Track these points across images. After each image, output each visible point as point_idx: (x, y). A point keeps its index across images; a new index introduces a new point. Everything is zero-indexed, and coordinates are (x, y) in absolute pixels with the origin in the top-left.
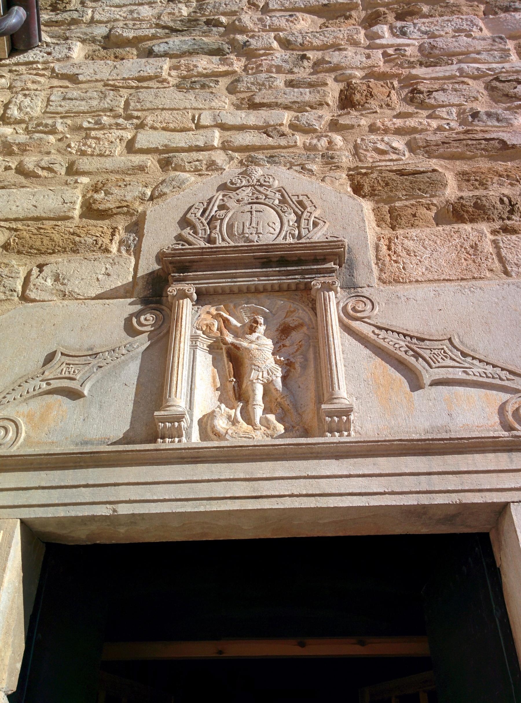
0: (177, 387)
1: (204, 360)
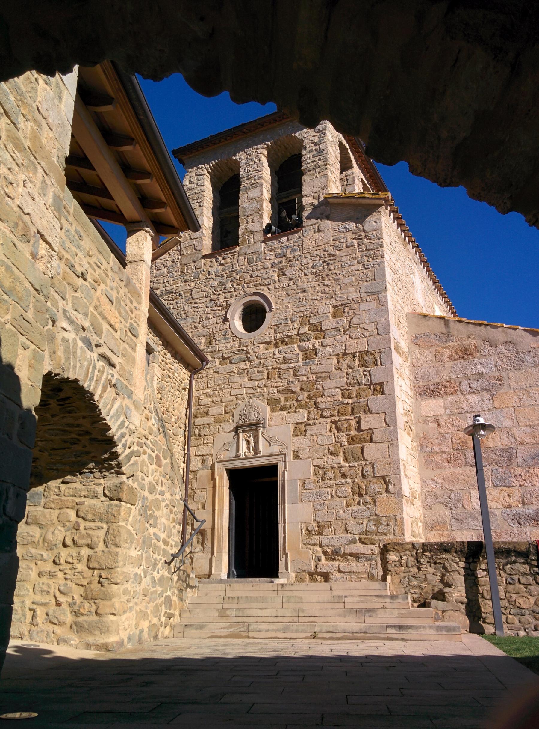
0: (183, 214)
1: (244, 442)
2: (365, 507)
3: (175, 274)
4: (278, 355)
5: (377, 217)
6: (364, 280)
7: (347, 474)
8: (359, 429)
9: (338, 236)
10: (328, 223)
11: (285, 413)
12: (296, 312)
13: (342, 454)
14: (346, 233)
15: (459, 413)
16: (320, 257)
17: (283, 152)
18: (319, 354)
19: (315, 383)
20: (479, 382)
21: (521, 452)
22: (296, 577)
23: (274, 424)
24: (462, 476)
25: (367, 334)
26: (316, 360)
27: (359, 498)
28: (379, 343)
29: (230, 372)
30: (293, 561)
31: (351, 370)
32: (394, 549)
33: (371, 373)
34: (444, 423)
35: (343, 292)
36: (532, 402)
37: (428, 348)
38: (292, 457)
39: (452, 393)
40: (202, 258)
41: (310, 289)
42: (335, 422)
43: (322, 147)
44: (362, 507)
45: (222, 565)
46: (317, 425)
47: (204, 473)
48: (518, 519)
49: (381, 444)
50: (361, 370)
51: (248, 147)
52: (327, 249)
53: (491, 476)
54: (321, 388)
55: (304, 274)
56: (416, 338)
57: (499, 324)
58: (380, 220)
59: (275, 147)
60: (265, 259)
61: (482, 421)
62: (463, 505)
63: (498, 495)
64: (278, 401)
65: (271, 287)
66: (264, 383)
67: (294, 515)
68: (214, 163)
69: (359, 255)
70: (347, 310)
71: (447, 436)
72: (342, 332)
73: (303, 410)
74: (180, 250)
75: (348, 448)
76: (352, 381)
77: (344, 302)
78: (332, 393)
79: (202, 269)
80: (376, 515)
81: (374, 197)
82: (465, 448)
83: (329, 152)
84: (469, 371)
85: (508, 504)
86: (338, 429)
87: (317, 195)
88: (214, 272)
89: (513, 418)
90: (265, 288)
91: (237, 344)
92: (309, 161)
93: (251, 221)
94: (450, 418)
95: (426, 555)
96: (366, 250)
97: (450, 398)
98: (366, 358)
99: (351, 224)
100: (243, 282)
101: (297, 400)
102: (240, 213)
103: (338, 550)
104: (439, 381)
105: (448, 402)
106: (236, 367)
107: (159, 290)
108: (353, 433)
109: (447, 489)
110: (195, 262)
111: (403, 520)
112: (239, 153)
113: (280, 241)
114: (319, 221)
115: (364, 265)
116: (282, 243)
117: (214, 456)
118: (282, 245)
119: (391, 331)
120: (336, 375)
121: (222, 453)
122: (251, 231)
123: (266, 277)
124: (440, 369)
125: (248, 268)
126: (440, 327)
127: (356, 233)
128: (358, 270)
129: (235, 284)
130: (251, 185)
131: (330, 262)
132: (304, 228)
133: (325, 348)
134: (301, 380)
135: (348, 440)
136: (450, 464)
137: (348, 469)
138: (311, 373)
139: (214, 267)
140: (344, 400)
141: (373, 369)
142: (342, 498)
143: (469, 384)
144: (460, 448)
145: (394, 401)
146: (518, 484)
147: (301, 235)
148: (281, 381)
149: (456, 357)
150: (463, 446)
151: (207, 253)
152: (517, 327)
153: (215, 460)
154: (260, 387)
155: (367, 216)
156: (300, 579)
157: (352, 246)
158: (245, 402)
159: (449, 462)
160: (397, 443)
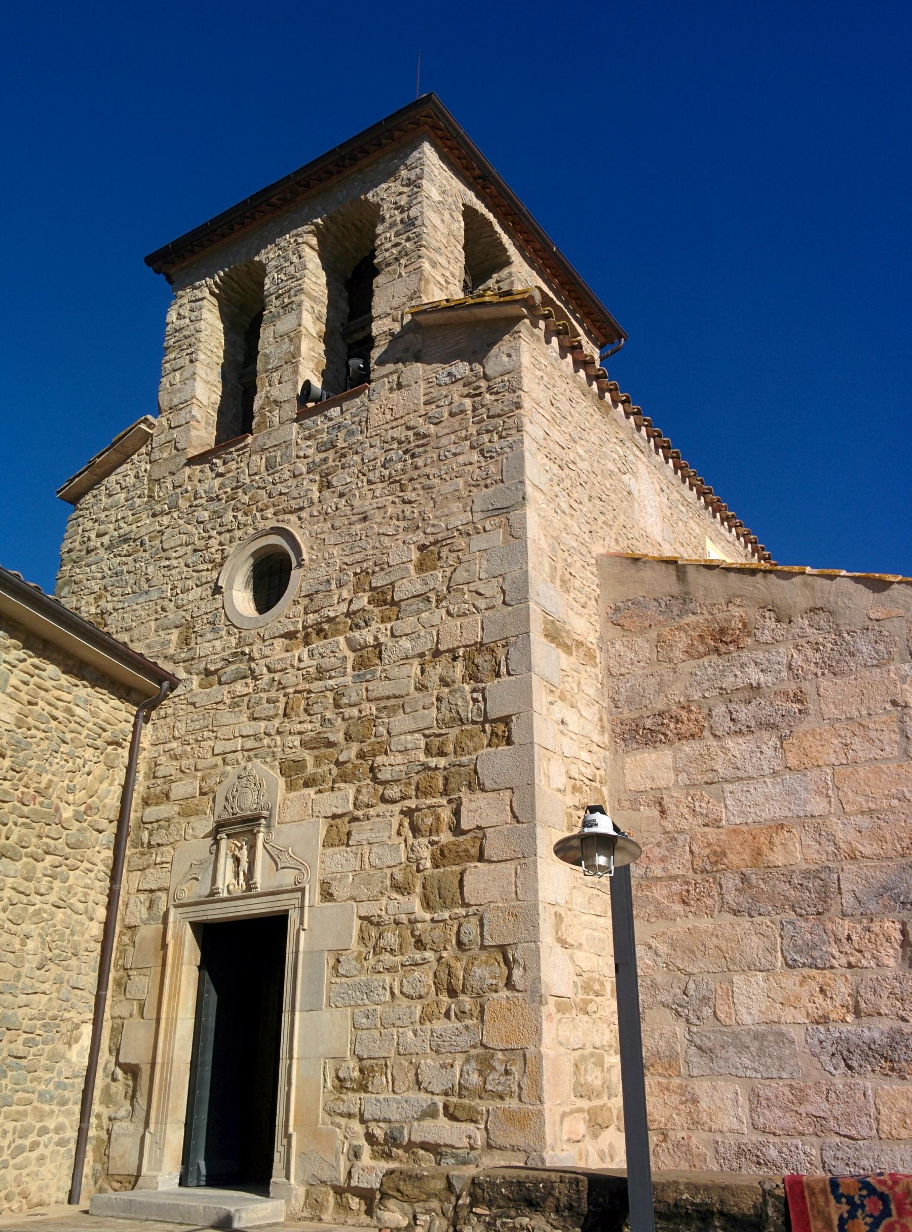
1: (230, 861)
2: (459, 1025)
3: (138, 501)
4: (307, 661)
5: (513, 344)
6: (482, 483)
7: (426, 939)
8: (456, 830)
9: (434, 395)
10: (419, 369)
11: (311, 791)
12: (346, 564)
13: (418, 889)
14: (451, 387)
15: (707, 783)
16: (400, 443)
17: (355, 239)
18: (384, 655)
19: (373, 721)
20: (752, 707)
21: (851, 879)
22: (307, 1197)
23: (288, 818)
24: (714, 939)
25: (482, 603)
26: (380, 668)
27: (450, 1000)
28: (505, 625)
29: (217, 703)
30: (302, 1154)
31: (446, 690)
32: (399, 1191)
33: (487, 695)
34: (674, 808)
35: (438, 513)
36: (875, 753)
37: (643, 631)
38: (318, 897)
39: (692, 736)
40: (186, 465)
41: (377, 511)
42: (408, 813)
43: (413, 213)
44: (454, 1024)
45: (162, 1156)
46: (372, 820)
47: (149, 932)
48: (845, 1053)
49: (499, 865)
50: (467, 688)
51: (281, 234)
52: (412, 424)
53: (779, 940)
54: (385, 733)
55: (368, 481)
56: (617, 609)
57: (796, 569)
58: (517, 350)
59: (333, 228)
60: (298, 457)
61: (604, 825)
62: (715, 1012)
63: (797, 988)
64: (300, 765)
65: (304, 514)
66: (277, 725)
67: (313, 1038)
68: (222, 273)
69: (473, 430)
70: (445, 552)
71: (681, 838)
72: (434, 604)
73: (347, 785)
74: (151, 452)
75: (432, 876)
76: (448, 715)
77: (439, 537)
78: (405, 747)
79: (184, 487)
80: (482, 1045)
81: (501, 299)
82: (720, 867)
83: (427, 222)
84: (728, 682)
85: (820, 1013)
86: (416, 830)
87: (400, 312)
88: (205, 492)
89: (830, 792)
90: (293, 518)
91: (233, 641)
92: (388, 245)
93: (276, 382)
94: (688, 794)
95: (479, 1216)
96: (488, 417)
97: (689, 748)
98: (479, 660)
99: (461, 364)
100: (254, 507)
101: (338, 763)
102: (259, 367)
103: (396, 1134)
104: (665, 708)
105: (683, 755)
106: (229, 692)
107: (107, 537)
108: (445, 837)
109: (679, 970)
110: (174, 474)
111: (541, 1061)
112: (266, 247)
113: (326, 417)
114: (400, 365)
115: (482, 452)
116: (330, 420)
117: (171, 891)
118: (330, 424)
119: (532, 594)
120: (416, 702)
121: (185, 887)
122: (275, 401)
123: (295, 493)
124: (666, 678)
125: (266, 477)
126: (667, 582)
127: (470, 383)
128: (471, 464)
129: (239, 514)
130: (282, 308)
131: (417, 450)
132: (373, 384)
133: (397, 642)
134: (347, 716)
135: (433, 854)
136: (687, 909)
137: (428, 925)
138: (369, 700)
139: (206, 481)
140: (430, 759)
141: (491, 685)
142: (412, 999)
143: (731, 713)
144: (708, 868)
145: (532, 761)
146: (844, 961)
147: (366, 400)
148: (309, 718)
149: (701, 649)
150: (716, 863)
151: (196, 453)
152: (836, 572)
153: (171, 903)
154: (269, 735)
155: (494, 344)
156: (314, 1205)
157: (462, 412)
158: (238, 770)
159: (684, 902)
160: (535, 862)
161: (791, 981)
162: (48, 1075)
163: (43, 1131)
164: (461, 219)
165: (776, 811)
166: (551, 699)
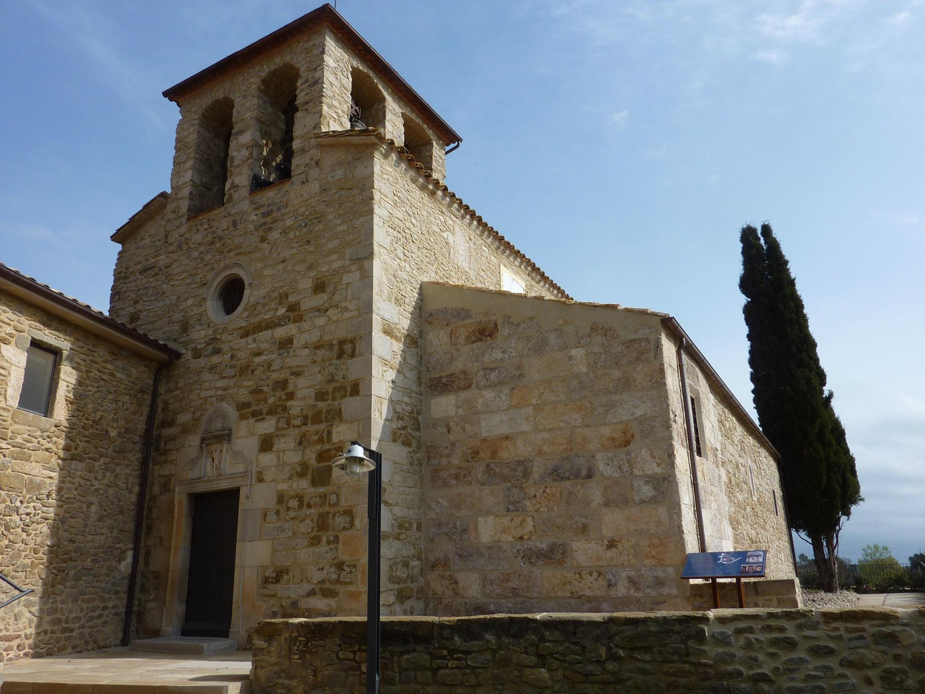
67: (252, 555)
97: (464, 395)
161: (506, 521)
162: (108, 579)
163: (105, 608)
164: (350, 76)
165: (504, 430)
166: (385, 369)
